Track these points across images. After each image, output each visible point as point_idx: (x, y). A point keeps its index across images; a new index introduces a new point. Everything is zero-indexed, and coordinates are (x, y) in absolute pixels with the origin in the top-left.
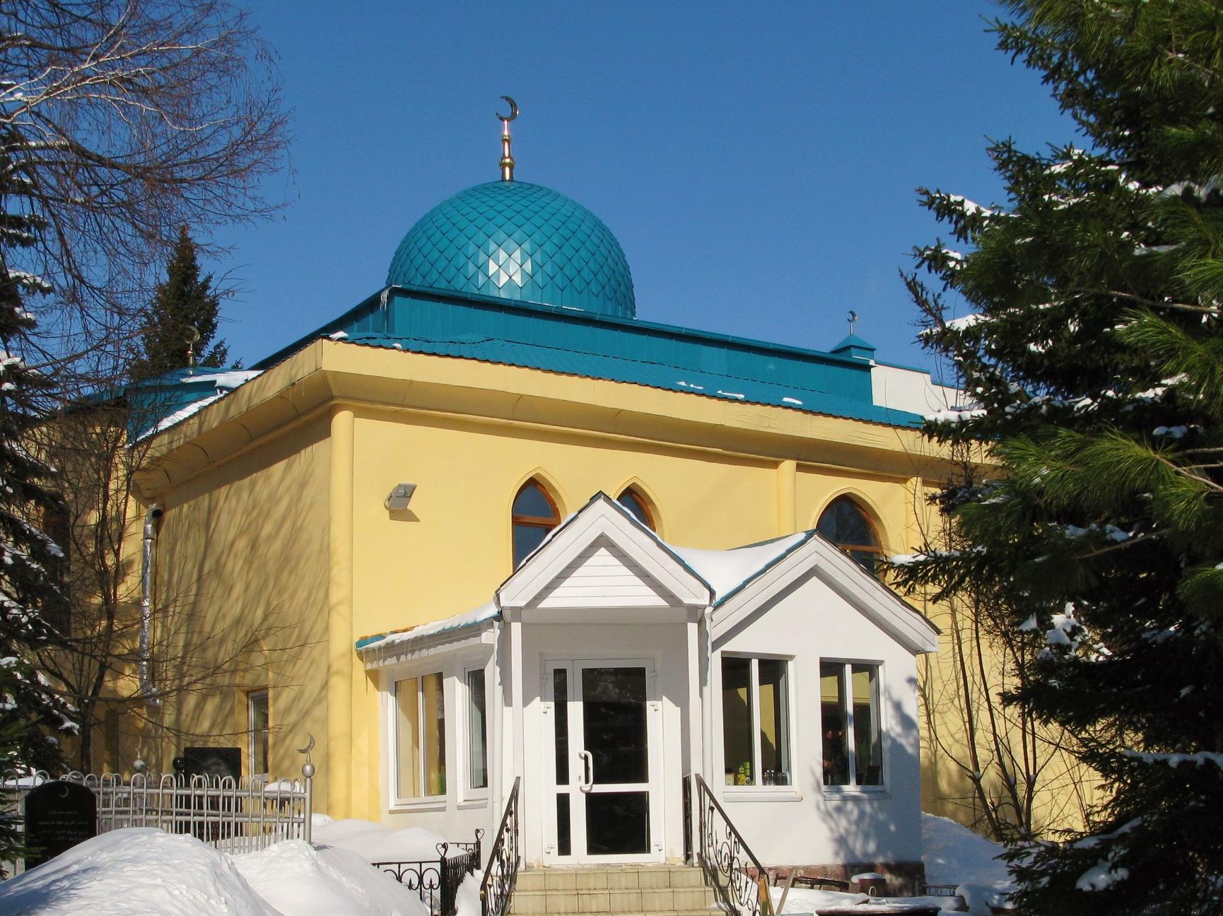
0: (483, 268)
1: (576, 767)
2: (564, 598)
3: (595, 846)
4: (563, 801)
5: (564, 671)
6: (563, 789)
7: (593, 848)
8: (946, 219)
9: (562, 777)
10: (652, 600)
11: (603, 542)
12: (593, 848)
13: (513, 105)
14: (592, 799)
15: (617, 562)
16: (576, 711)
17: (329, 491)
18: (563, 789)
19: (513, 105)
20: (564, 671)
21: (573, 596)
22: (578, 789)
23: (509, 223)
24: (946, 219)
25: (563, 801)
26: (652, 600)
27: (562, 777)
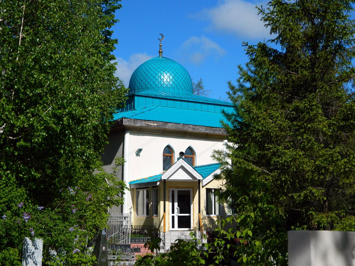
0: (160, 77)
1: (176, 211)
2: (173, 178)
3: (179, 226)
4: (173, 217)
5: (174, 191)
6: (173, 215)
7: (179, 227)
8: (113, 37)
9: (173, 212)
10: (189, 178)
11: (182, 167)
12: (179, 227)
13: (162, 35)
14: (179, 217)
15: (184, 172)
16: (176, 204)
17: (197, 138)
18: (173, 215)
19: (162, 35)
20: (174, 191)
21: (175, 177)
22: (176, 214)
23: (163, 69)
24: (113, 37)
25: (173, 217)
26: (189, 178)
27: (173, 212)
